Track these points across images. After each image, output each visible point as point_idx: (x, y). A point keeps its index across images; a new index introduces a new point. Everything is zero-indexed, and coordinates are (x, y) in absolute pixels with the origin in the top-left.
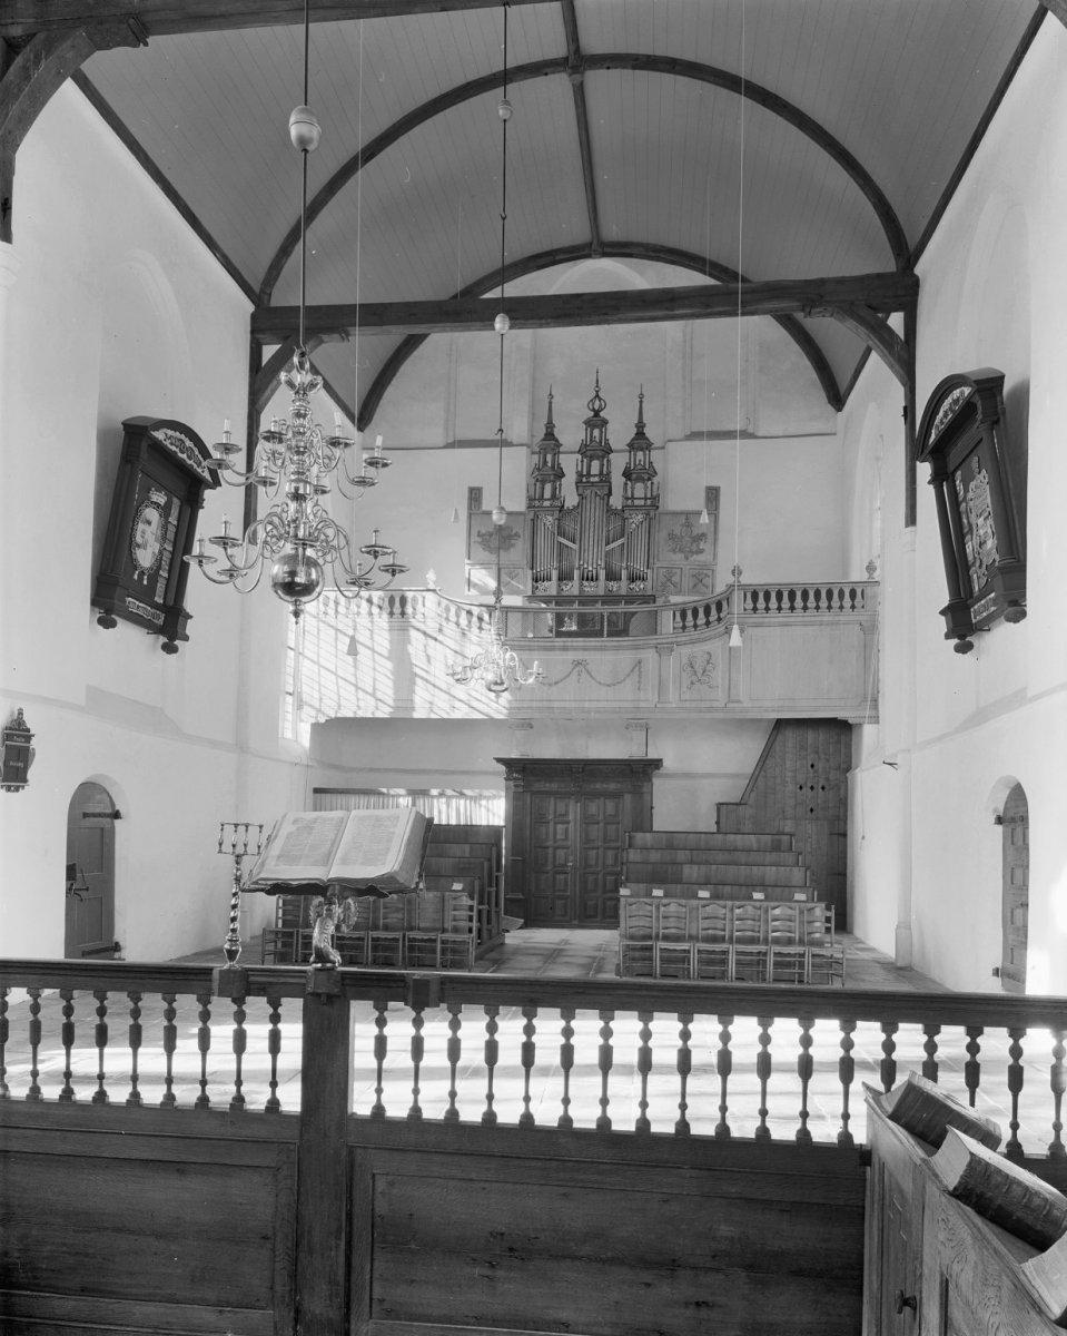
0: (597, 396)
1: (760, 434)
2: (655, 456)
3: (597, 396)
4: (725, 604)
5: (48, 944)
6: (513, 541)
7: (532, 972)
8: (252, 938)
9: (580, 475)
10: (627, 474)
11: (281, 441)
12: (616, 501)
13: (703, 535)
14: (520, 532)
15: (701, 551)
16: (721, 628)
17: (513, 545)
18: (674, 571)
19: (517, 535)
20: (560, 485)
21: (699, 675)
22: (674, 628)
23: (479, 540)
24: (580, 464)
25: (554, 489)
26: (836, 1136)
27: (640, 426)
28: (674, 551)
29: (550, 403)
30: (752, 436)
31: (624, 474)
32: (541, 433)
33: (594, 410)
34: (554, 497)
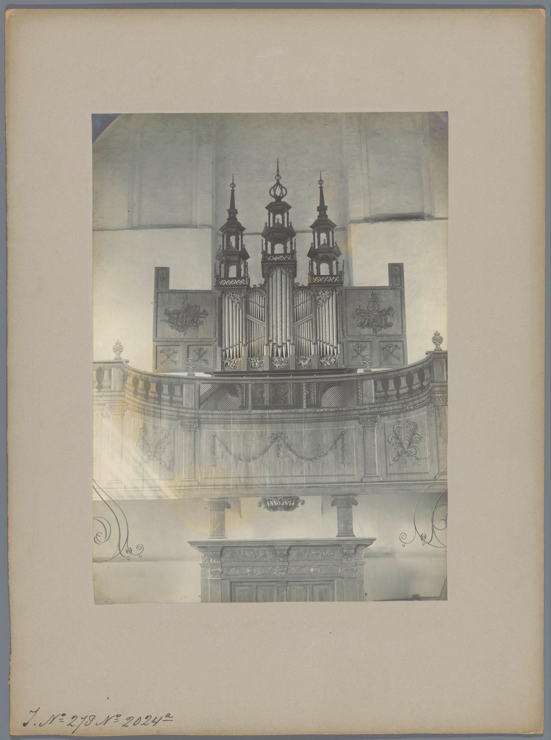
0: (278, 184)
1: (437, 216)
2: (337, 236)
3: (278, 184)
4: (426, 373)
5: (328, 274)
6: (201, 319)
7: (149, 405)
8: (247, 263)
9: (265, 253)
10: (313, 254)
11: (313, 584)
12: (302, 278)
13: (390, 309)
14: (208, 310)
15: (389, 325)
16: (424, 397)
17: (202, 323)
18: (364, 344)
19: (205, 313)
20: (246, 266)
21: (405, 446)
22: (376, 398)
23: (167, 318)
24: (264, 246)
25: (239, 271)
26: (132, 382)
27: (322, 209)
28: (362, 325)
29: (233, 192)
30: (431, 217)
31: (309, 255)
32: (224, 217)
33: (275, 196)
34: (239, 276)
